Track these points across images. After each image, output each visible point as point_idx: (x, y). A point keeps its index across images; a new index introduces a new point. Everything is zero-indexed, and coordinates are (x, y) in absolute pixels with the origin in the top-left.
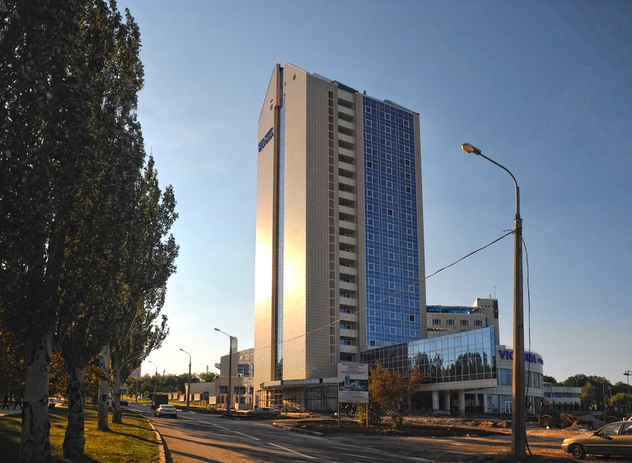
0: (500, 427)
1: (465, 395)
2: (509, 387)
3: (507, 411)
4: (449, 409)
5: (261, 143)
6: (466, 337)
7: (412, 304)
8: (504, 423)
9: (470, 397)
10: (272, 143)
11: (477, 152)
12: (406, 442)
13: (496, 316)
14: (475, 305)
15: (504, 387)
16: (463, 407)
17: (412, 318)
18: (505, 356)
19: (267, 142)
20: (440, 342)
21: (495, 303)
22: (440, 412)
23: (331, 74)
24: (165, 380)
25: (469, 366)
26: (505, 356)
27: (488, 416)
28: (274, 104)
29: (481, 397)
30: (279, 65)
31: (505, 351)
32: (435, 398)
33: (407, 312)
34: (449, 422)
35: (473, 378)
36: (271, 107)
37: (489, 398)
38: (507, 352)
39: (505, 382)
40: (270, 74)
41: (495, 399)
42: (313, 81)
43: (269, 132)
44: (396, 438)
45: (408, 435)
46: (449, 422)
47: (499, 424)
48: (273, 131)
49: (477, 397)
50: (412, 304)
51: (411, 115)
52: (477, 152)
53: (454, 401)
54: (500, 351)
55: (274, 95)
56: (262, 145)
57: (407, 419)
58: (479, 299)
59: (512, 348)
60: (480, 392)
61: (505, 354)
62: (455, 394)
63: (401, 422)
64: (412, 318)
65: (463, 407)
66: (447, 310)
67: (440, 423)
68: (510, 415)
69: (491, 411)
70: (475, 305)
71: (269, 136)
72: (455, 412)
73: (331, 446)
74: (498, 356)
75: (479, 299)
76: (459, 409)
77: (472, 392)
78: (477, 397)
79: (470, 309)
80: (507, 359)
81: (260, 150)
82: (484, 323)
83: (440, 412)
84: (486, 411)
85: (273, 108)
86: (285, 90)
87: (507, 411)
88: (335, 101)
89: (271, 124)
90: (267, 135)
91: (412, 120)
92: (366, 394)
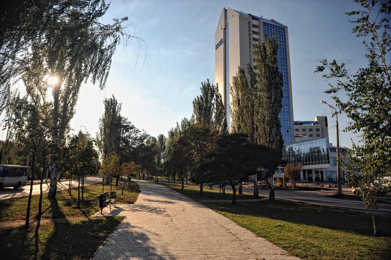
0: (332, 187)
1: (315, 171)
2: (335, 166)
3: (335, 180)
4: (307, 179)
5: (217, 46)
6: (315, 143)
7: (287, 124)
8: (333, 185)
9: (317, 172)
10: (222, 45)
11: (326, 103)
12: (302, 192)
13: (327, 126)
14: (316, 120)
15: (333, 166)
16: (314, 178)
17: (288, 131)
18: (333, 151)
19: (220, 45)
20: (303, 145)
21: (326, 118)
22: (304, 181)
23: (246, 11)
24: (4, 144)
25: (315, 156)
26: (333, 151)
27: (326, 182)
28: (223, 27)
29: (322, 172)
30: (225, 8)
31: (332, 148)
32: (302, 173)
33: (285, 128)
34: (310, 185)
35: (319, 163)
36: (222, 28)
37: (326, 173)
38: (333, 148)
39: (333, 164)
40: (221, 12)
41: (329, 174)
42: (242, 16)
43: (221, 41)
44: (297, 191)
45: (301, 190)
46: (310, 185)
47: (332, 186)
48: (223, 40)
49: (320, 172)
50: (287, 124)
51: (284, 28)
52: (326, 103)
53: (309, 174)
54: (330, 148)
55: (223, 23)
56: (217, 47)
57: (297, 184)
58: (317, 117)
59: (335, 146)
60: (321, 170)
61: (333, 149)
62: (310, 171)
63: (295, 185)
64: (288, 131)
65: (314, 178)
66: (301, 123)
67: (14, 195)
68: (336, 182)
69: (327, 180)
70: (316, 120)
71: (221, 42)
72: (310, 180)
73: (196, 207)
74: (329, 150)
75: (317, 117)
76: (313, 179)
77: (318, 170)
78: (320, 172)
79: (313, 122)
80: (334, 152)
81: (216, 49)
82: (321, 135)
83: (304, 181)
84: (324, 180)
85: (223, 29)
86: (229, 21)
87: (335, 180)
88: (251, 26)
89: (222, 37)
90: (220, 42)
91: (284, 30)
92: (283, 174)
